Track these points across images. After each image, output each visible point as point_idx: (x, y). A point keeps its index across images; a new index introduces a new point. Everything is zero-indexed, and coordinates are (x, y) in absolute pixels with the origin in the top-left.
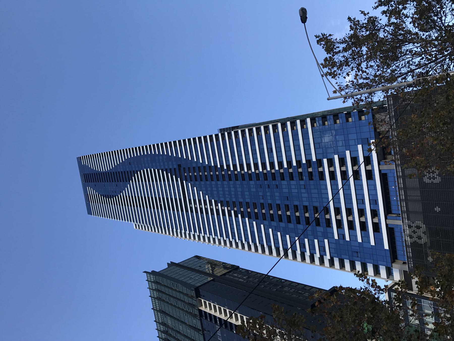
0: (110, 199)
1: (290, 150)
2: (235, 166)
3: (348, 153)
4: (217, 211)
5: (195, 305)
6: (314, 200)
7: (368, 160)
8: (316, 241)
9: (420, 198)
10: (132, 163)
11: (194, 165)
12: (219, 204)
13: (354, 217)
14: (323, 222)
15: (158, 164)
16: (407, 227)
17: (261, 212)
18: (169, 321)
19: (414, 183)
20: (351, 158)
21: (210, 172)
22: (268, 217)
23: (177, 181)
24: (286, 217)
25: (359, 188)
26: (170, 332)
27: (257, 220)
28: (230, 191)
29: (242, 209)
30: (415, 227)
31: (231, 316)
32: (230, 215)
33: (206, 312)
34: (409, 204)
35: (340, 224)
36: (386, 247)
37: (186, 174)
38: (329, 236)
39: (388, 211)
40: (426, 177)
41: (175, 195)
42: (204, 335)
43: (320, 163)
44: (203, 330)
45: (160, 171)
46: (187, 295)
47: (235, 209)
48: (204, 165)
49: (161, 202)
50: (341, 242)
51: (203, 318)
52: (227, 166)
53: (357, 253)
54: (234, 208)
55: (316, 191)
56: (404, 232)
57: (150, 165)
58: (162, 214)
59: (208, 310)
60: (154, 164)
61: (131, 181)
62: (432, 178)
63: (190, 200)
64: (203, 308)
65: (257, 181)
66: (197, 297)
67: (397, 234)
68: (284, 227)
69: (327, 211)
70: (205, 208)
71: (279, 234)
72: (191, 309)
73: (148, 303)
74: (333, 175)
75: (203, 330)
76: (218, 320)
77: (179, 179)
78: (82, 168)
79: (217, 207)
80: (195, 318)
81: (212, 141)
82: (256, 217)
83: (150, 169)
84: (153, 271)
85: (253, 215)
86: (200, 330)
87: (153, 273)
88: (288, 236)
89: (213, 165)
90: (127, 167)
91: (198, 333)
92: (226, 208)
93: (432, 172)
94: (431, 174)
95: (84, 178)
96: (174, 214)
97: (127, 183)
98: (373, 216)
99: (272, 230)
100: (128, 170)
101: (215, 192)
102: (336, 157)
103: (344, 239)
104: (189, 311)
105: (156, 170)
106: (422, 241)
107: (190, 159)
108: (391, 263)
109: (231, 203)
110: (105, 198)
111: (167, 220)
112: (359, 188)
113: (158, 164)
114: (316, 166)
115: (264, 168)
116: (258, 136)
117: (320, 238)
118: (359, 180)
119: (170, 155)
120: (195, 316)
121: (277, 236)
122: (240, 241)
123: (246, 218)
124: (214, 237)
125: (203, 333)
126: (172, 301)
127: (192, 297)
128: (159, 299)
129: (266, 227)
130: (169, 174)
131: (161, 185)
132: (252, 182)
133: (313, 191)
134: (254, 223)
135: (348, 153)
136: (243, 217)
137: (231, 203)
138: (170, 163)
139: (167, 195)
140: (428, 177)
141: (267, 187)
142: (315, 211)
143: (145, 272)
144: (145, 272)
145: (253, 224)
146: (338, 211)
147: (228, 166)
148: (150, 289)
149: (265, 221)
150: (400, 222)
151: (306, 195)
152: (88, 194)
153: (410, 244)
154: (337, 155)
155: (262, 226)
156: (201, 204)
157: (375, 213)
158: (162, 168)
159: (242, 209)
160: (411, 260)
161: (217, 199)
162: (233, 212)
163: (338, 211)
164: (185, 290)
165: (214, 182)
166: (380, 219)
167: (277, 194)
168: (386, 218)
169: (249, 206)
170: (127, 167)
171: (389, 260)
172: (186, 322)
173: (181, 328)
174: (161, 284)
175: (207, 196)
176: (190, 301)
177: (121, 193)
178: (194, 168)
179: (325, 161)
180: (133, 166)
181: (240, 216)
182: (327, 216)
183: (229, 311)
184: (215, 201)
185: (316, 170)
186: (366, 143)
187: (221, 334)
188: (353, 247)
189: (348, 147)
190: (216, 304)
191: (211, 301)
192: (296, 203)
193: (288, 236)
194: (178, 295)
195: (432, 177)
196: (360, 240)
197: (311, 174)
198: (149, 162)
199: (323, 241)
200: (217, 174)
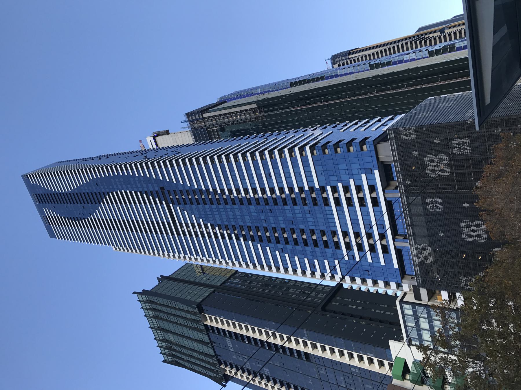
0: (80, 221)
1: (312, 176)
2: (230, 191)
3: (352, 182)
4: (215, 234)
5: (199, 320)
6: (320, 224)
7: (372, 188)
8: (326, 262)
9: (424, 223)
10: (100, 183)
11: (181, 188)
12: (217, 228)
13: (387, 241)
14: (331, 244)
15: (134, 186)
16: (414, 249)
17: (301, 238)
18: (171, 338)
19: (419, 210)
20: (356, 186)
21: (176, 196)
22: (273, 240)
23: (161, 204)
24: (333, 243)
25: (365, 214)
26: (174, 347)
27: (261, 243)
28: (227, 215)
29: (243, 233)
30: (422, 249)
31: (289, 340)
32: (230, 238)
33: (213, 326)
34: (415, 228)
35: (348, 246)
36: (396, 266)
37: (171, 197)
38: (339, 257)
39: (395, 234)
40: (429, 205)
41: (161, 218)
42: (213, 348)
43: (323, 189)
44: (212, 342)
45: (139, 193)
46: (188, 312)
47: (236, 232)
48: (193, 189)
49: (145, 225)
50: (352, 262)
51: (210, 332)
52: (220, 190)
53: (368, 271)
54: (234, 231)
55: (322, 216)
56: (412, 254)
57: (124, 186)
58: (148, 237)
59: (214, 324)
60: (129, 186)
61: (102, 203)
62: (435, 207)
63: (181, 224)
64: (208, 323)
65: (258, 206)
66: (200, 313)
67: (404, 253)
68: (291, 249)
69: (335, 233)
70: (194, 231)
71: (287, 255)
72: (190, 323)
73: (145, 323)
74: (338, 202)
75: (212, 342)
76: (227, 332)
77: (164, 202)
78: (32, 188)
79: (208, 230)
80: (191, 330)
81: (186, 165)
82: (261, 240)
83: (120, 191)
84: (144, 291)
85: (265, 239)
86: (208, 343)
87: (145, 292)
88: (296, 258)
89: (204, 188)
90: (94, 188)
91: (206, 347)
92: (225, 232)
93: (434, 202)
94: (434, 203)
95: (37, 199)
96: (158, 238)
97: (97, 205)
98: (368, 237)
99: (279, 252)
100: (95, 191)
101: (210, 216)
102: (340, 185)
103: (354, 260)
104: (193, 326)
105: (133, 192)
106: (428, 261)
107: (175, 182)
108: (401, 280)
109: (230, 227)
110: (74, 221)
111: (155, 243)
112: (365, 214)
113: (134, 186)
114: (320, 192)
115: (263, 193)
116: (206, 165)
117: (329, 259)
118: (365, 206)
119: (148, 176)
120: (201, 331)
121: (284, 257)
122: (230, 261)
123: (249, 241)
124: (190, 256)
125: (212, 346)
126: (172, 318)
127: (195, 314)
128: (155, 317)
129: (272, 249)
130: (151, 197)
131: (132, 208)
132: (252, 207)
133: (318, 216)
134: (259, 246)
135: (352, 182)
136: (245, 240)
137: (230, 227)
138: (150, 185)
139: (136, 217)
140: (431, 205)
141: (269, 212)
142: (302, 232)
143: (135, 293)
144: (135, 293)
145: (257, 246)
146: (346, 234)
147: (222, 190)
148: (143, 308)
149: (270, 244)
150: (407, 245)
151: (312, 220)
152: (46, 216)
153: (417, 263)
154: (341, 183)
155: (268, 248)
156: (189, 227)
157: (382, 236)
158: (140, 190)
159: (243, 233)
160: (420, 277)
161: (213, 223)
162: (233, 235)
163: (346, 234)
164: (186, 308)
165: (230, 206)
166: (339, 239)
167: (281, 218)
168: (394, 241)
169: (251, 229)
170: (94, 188)
171: (399, 276)
172: (191, 337)
173: (186, 343)
174: (155, 302)
175: (201, 220)
176: (194, 317)
177: (92, 216)
178: (181, 191)
179: (329, 188)
180: (102, 187)
181: (242, 239)
182: (336, 239)
183: (311, 343)
184: (211, 225)
185: (289, 197)
186: (369, 172)
187: (232, 345)
188: (363, 267)
189: (351, 176)
190: (223, 317)
191: (217, 316)
192: (302, 227)
193: (296, 258)
194: (178, 313)
195: (435, 206)
196: (370, 260)
197: (314, 200)
198: (142, 182)
199: (333, 261)
200: (224, 197)
